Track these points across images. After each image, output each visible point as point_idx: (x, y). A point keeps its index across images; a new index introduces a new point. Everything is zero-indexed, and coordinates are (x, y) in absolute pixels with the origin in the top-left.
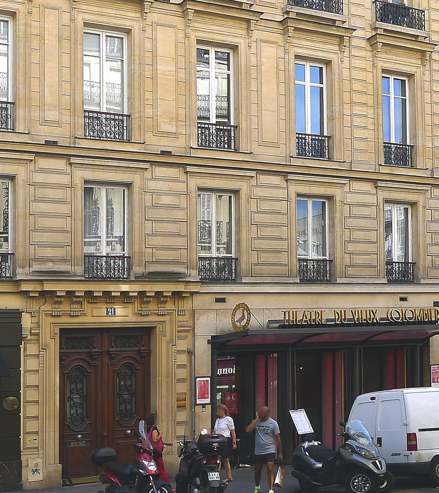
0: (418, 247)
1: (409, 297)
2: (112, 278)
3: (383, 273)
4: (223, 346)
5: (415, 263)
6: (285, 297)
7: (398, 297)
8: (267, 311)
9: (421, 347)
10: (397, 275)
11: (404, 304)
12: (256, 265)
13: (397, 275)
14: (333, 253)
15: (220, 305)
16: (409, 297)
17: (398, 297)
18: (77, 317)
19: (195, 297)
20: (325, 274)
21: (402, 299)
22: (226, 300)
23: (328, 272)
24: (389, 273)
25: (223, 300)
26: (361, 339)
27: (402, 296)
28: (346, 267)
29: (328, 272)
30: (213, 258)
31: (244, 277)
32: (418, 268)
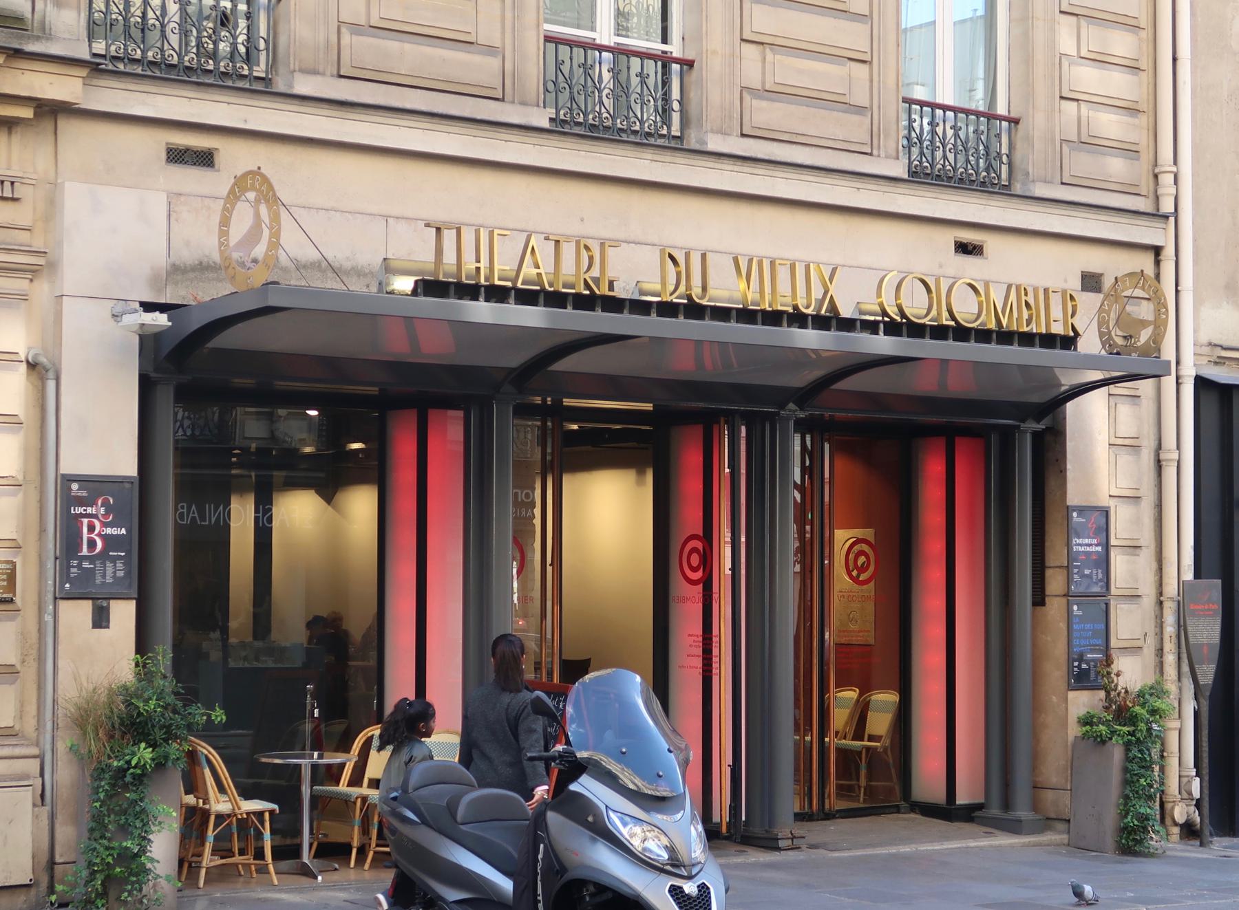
0: (1028, 61)
1: (991, 243)
2: (243, 77)
3: (893, 139)
4: (802, 409)
5: (1016, 122)
6: (488, 179)
7: (948, 237)
8: (402, 227)
9: (1037, 437)
10: (951, 157)
11: (970, 267)
12: (356, 29)
13: (951, 157)
14: (694, 36)
15: (190, 178)
16: (991, 243)
17: (948, 237)
18: (10, 204)
19: (69, 128)
20: (995, 164)
21: (964, 248)
22: (219, 159)
23: (1005, 159)
24: (557, 85)
25: (205, 159)
26: (515, 360)
27: (968, 236)
28: (747, 96)
29: (1005, 159)
30: (602, 48)
31: (302, 71)
32: (1029, 140)
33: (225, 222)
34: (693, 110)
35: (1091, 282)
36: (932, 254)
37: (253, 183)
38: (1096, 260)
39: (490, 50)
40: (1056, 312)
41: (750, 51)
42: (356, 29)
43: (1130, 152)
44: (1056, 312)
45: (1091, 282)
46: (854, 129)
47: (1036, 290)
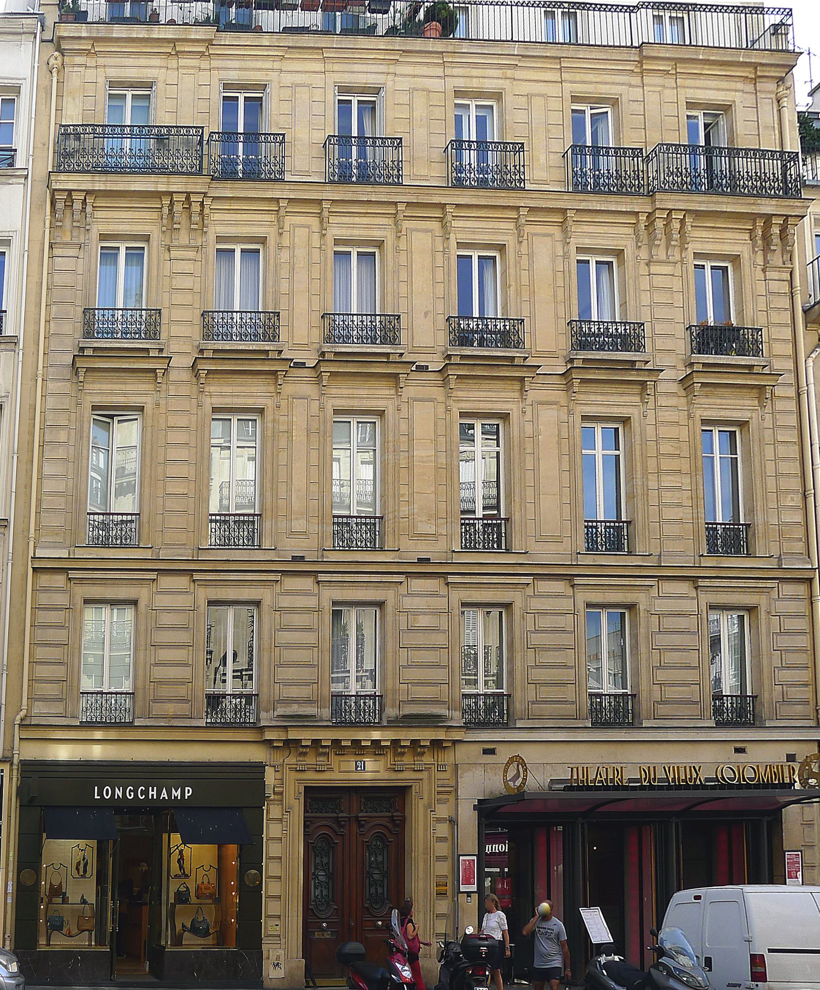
0: (761, 671)
3: (710, 711)
4: (490, 813)
6: (572, 747)
9: (769, 823)
12: (533, 703)
14: (636, 685)
15: (489, 758)
21: (737, 750)
22: (497, 751)
25: (492, 752)
33: (506, 771)
34: (636, 711)
35: (791, 758)
36: (726, 755)
37: (519, 761)
38: (791, 749)
39: (572, 703)
40: (786, 774)
41: (657, 687)
42: (533, 703)
43: (806, 703)
44: (786, 774)
45: (791, 758)
46: (695, 710)
47: (109, 354)
